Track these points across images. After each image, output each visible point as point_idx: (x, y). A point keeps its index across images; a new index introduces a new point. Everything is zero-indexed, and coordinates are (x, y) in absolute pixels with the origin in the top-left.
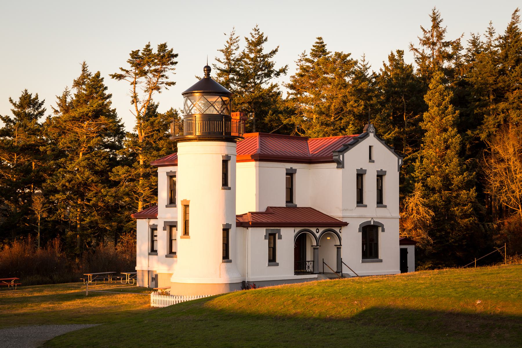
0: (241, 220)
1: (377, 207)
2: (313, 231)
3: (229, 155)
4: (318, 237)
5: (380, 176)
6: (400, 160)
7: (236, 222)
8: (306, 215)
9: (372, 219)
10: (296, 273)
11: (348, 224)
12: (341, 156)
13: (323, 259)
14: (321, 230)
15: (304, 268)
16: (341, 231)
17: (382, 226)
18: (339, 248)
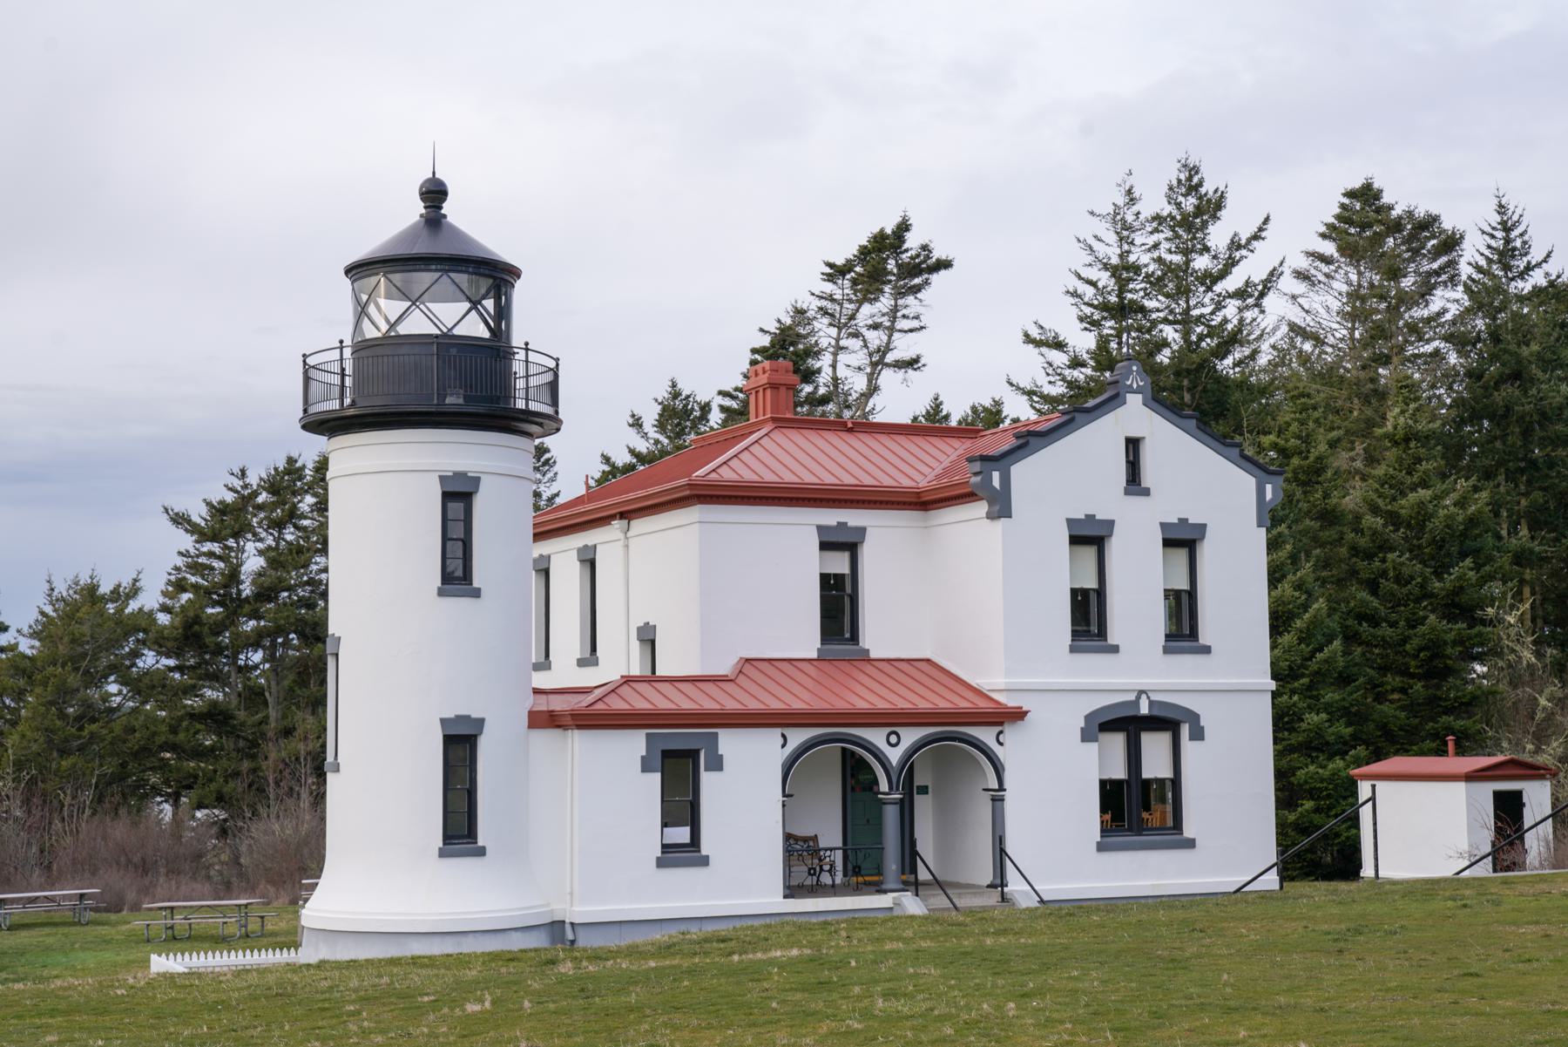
1: (1073, 650)
3: (469, 474)
6: (1269, 488)
10: (791, 891)
11: (1026, 713)
12: (996, 476)
14: (910, 736)
15: (892, 865)
16: (1001, 739)
17: (1193, 718)
18: (997, 800)
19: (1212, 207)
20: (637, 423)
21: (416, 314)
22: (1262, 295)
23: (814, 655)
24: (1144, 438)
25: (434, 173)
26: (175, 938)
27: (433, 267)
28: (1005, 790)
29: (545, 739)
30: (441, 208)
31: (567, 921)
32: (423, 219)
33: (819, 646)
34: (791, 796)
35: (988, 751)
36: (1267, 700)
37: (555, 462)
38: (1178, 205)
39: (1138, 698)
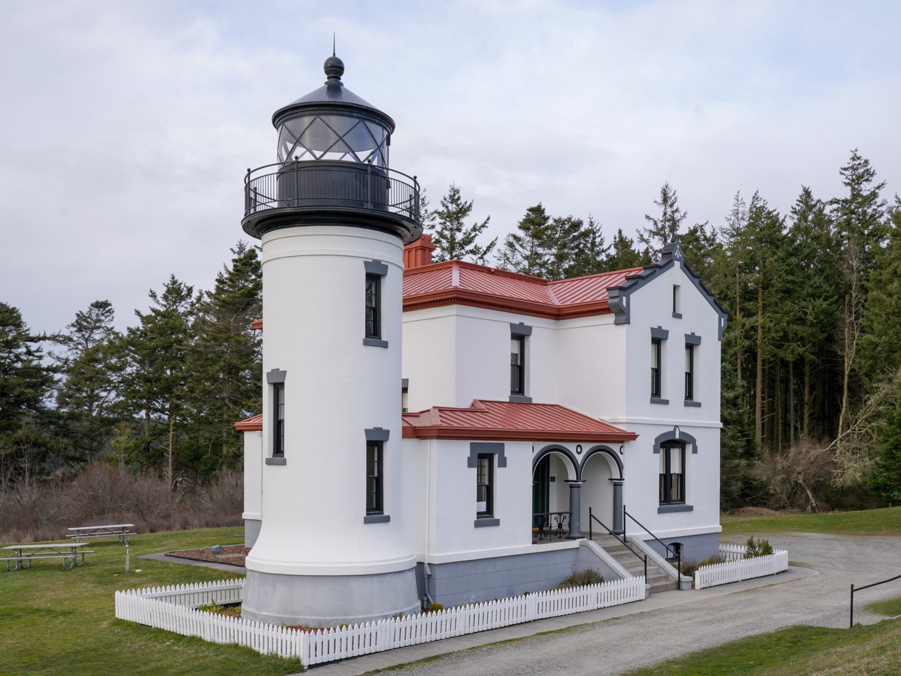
0: (415, 423)
2: (567, 447)
3: (382, 263)
4: (580, 463)
5: (691, 345)
7: (403, 427)
8: (483, 420)
9: (677, 429)
11: (637, 436)
12: (624, 298)
13: (590, 509)
14: (587, 447)
17: (693, 441)
18: (617, 485)
19: (463, 211)
20: (153, 295)
21: (318, 156)
22: (485, 253)
23: (508, 400)
24: (679, 286)
25: (334, 54)
26: (22, 568)
27: (355, 115)
28: (624, 480)
29: (412, 443)
30: (340, 79)
31: (426, 562)
32: (327, 86)
33: (510, 395)
34: (585, 481)
35: (574, 460)
36: (718, 433)
37: (113, 312)
38: (447, 207)
39: (675, 430)
